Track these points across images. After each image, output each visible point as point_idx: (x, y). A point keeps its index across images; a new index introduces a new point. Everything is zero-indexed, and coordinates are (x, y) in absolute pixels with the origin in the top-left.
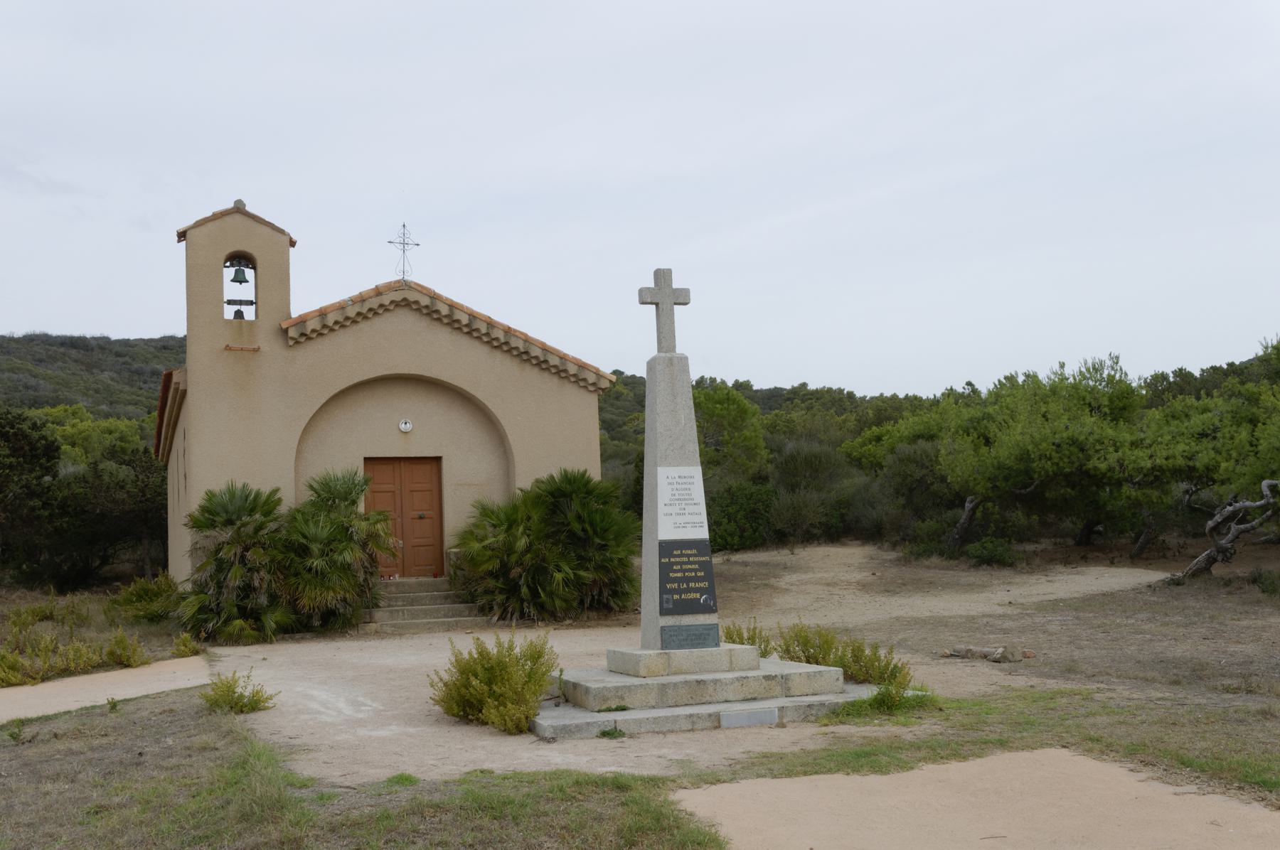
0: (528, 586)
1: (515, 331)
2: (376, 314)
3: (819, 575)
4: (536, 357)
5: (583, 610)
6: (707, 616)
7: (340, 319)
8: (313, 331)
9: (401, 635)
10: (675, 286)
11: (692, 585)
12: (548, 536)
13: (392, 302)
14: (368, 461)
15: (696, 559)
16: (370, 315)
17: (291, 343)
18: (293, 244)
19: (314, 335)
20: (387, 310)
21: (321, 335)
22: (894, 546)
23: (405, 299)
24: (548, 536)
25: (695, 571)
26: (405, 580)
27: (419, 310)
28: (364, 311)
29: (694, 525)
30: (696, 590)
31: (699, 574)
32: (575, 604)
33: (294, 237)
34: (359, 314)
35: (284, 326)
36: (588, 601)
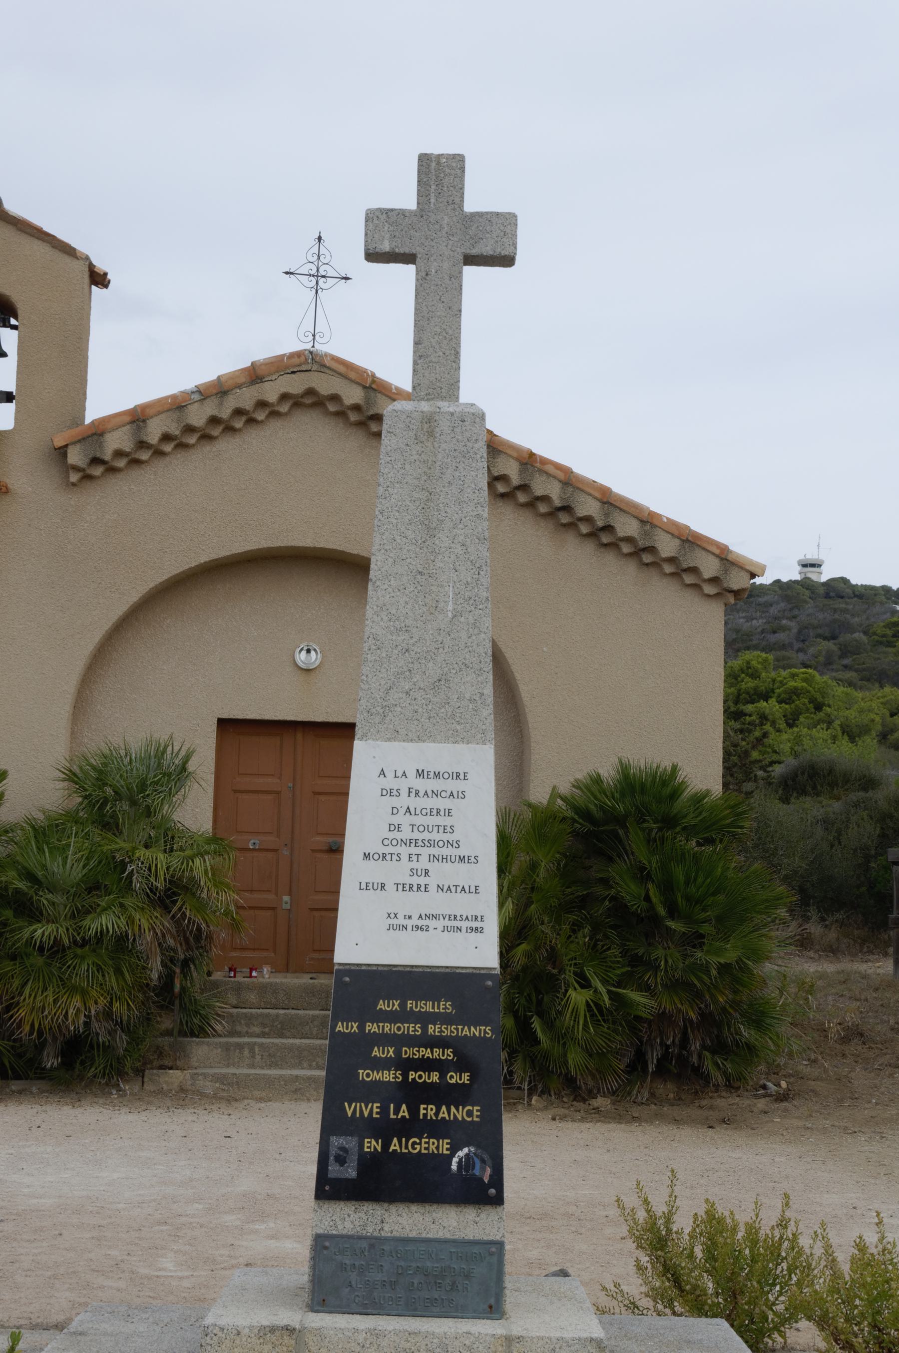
1: (545, 461)
2: (251, 421)
4: (588, 519)
7: (174, 430)
8: (119, 454)
9: (230, 1100)
10: (471, 205)
13: (284, 397)
14: (223, 723)
15: (448, 1031)
16: (238, 424)
17: (74, 477)
18: (99, 279)
19: (121, 463)
20: (274, 414)
21: (136, 462)
23: (310, 392)
26: (280, 979)
27: (341, 414)
28: (225, 414)
29: (455, 923)
31: (454, 1078)
33: (101, 265)
34: (214, 421)
35: (59, 442)
36: (653, 1058)
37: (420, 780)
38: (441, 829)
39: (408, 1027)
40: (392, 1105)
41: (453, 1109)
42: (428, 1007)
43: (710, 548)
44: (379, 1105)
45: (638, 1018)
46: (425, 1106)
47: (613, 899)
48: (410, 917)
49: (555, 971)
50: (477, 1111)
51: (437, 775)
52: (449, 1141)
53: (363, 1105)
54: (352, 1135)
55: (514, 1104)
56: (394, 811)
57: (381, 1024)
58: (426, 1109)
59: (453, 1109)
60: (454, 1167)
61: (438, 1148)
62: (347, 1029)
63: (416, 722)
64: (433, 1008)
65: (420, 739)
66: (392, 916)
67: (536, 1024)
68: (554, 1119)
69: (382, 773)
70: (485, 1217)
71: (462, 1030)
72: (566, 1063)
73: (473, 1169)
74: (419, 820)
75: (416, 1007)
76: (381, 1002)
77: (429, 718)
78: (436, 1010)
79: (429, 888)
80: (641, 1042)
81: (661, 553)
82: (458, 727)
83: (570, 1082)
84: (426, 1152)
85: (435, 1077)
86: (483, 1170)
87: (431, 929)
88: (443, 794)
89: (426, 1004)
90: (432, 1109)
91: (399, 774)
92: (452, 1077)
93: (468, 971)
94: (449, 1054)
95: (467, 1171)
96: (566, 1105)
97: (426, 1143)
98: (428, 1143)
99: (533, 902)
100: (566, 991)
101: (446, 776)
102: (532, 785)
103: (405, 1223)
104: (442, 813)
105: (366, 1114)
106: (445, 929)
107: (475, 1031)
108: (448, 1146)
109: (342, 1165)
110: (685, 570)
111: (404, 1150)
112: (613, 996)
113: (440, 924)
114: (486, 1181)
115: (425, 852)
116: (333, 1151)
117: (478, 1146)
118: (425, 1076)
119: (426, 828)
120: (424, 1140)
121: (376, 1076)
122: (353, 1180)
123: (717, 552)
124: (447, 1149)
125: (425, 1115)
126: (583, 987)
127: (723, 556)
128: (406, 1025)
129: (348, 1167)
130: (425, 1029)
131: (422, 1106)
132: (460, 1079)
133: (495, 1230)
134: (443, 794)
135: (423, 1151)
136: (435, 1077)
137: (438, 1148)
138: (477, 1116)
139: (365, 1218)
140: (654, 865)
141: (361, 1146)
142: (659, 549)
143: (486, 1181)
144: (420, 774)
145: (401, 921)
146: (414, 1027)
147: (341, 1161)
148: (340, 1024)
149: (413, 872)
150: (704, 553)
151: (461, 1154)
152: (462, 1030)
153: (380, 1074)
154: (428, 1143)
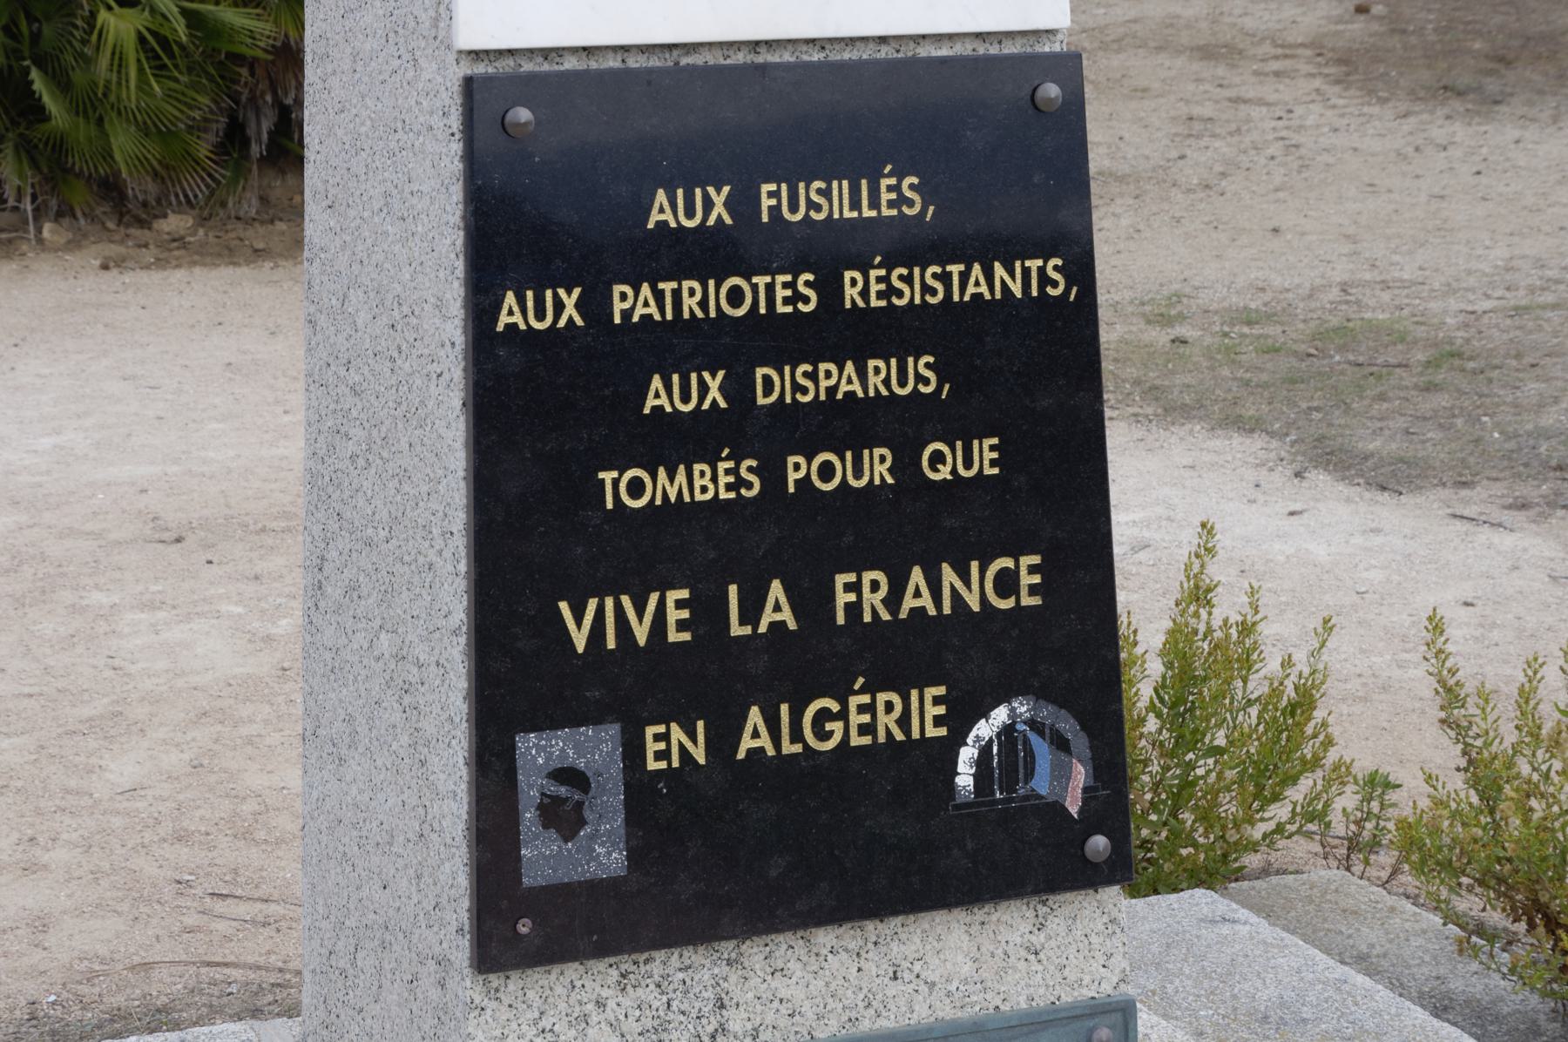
5: (240, 172)
6: (1012, 923)
11: (861, 593)
15: (918, 287)
25: (896, 422)
30: (898, 654)
31: (944, 464)
32: (203, 150)
39: (770, 288)
40: (733, 590)
41: (949, 575)
42: (832, 202)
44: (684, 594)
46: (851, 577)
50: (1032, 570)
52: (941, 690)
53: (626, 600)
54: (597, 720)
55: (10, 241)
57: (667, 287)
58: (855, 587)
59: (949, 575)
60: (965, 779)
61: (905, 722)
62: (540, 316)
64: (855, 204)
67: (38, 83)
68: (105, 267)
70: (1062, 930)
71: (965, 277)
72: (108, 155)
73: (1030, 774)
75: (794, 208)
76: (661, 196)
78: (868, 213)
80: (237, 103)
83: (111, 189)
84: (866, 740)
85: (879, 466)
86: (1061, 775)
89: (826, 193)
90: (875, 586)
92: (937, 458)
93: (959, 49)
94: (921, 375)
95: (1009, 787)
96: (117, 237)
97: (862, 709)
98: (869, 708)
100: (93, 15)
103: (798, 994)
105: (641, 634)
107: (1008, 280)
108: (941, 710)
109: (569, 834)
111: (789, 748)
114: (1074, 810)
116: (532, 787)
117: (1041, 693)
118: (843, 468)
120: (854, 701)
121: (667, 486)
122: (614, 883)
124: (938, 721)
125: (854, 609)
128: (761, 281)
129: (593, 837)
130: (829, 288)
131: (841, 579)
132: (968, 464)
133: (1096, 966)
135: (856, 741)
136: (879, 466)
137: (905, 722)
138: (1033, 590)
139: (659, 1002)
141: (633, 751)
143: (1074, 810)
146: (790, 285)
147: (563, 818)
148: (510, 298)
151: (984, 729)
152: (965, 277)
153: (681, 477)
154: (869, 708)
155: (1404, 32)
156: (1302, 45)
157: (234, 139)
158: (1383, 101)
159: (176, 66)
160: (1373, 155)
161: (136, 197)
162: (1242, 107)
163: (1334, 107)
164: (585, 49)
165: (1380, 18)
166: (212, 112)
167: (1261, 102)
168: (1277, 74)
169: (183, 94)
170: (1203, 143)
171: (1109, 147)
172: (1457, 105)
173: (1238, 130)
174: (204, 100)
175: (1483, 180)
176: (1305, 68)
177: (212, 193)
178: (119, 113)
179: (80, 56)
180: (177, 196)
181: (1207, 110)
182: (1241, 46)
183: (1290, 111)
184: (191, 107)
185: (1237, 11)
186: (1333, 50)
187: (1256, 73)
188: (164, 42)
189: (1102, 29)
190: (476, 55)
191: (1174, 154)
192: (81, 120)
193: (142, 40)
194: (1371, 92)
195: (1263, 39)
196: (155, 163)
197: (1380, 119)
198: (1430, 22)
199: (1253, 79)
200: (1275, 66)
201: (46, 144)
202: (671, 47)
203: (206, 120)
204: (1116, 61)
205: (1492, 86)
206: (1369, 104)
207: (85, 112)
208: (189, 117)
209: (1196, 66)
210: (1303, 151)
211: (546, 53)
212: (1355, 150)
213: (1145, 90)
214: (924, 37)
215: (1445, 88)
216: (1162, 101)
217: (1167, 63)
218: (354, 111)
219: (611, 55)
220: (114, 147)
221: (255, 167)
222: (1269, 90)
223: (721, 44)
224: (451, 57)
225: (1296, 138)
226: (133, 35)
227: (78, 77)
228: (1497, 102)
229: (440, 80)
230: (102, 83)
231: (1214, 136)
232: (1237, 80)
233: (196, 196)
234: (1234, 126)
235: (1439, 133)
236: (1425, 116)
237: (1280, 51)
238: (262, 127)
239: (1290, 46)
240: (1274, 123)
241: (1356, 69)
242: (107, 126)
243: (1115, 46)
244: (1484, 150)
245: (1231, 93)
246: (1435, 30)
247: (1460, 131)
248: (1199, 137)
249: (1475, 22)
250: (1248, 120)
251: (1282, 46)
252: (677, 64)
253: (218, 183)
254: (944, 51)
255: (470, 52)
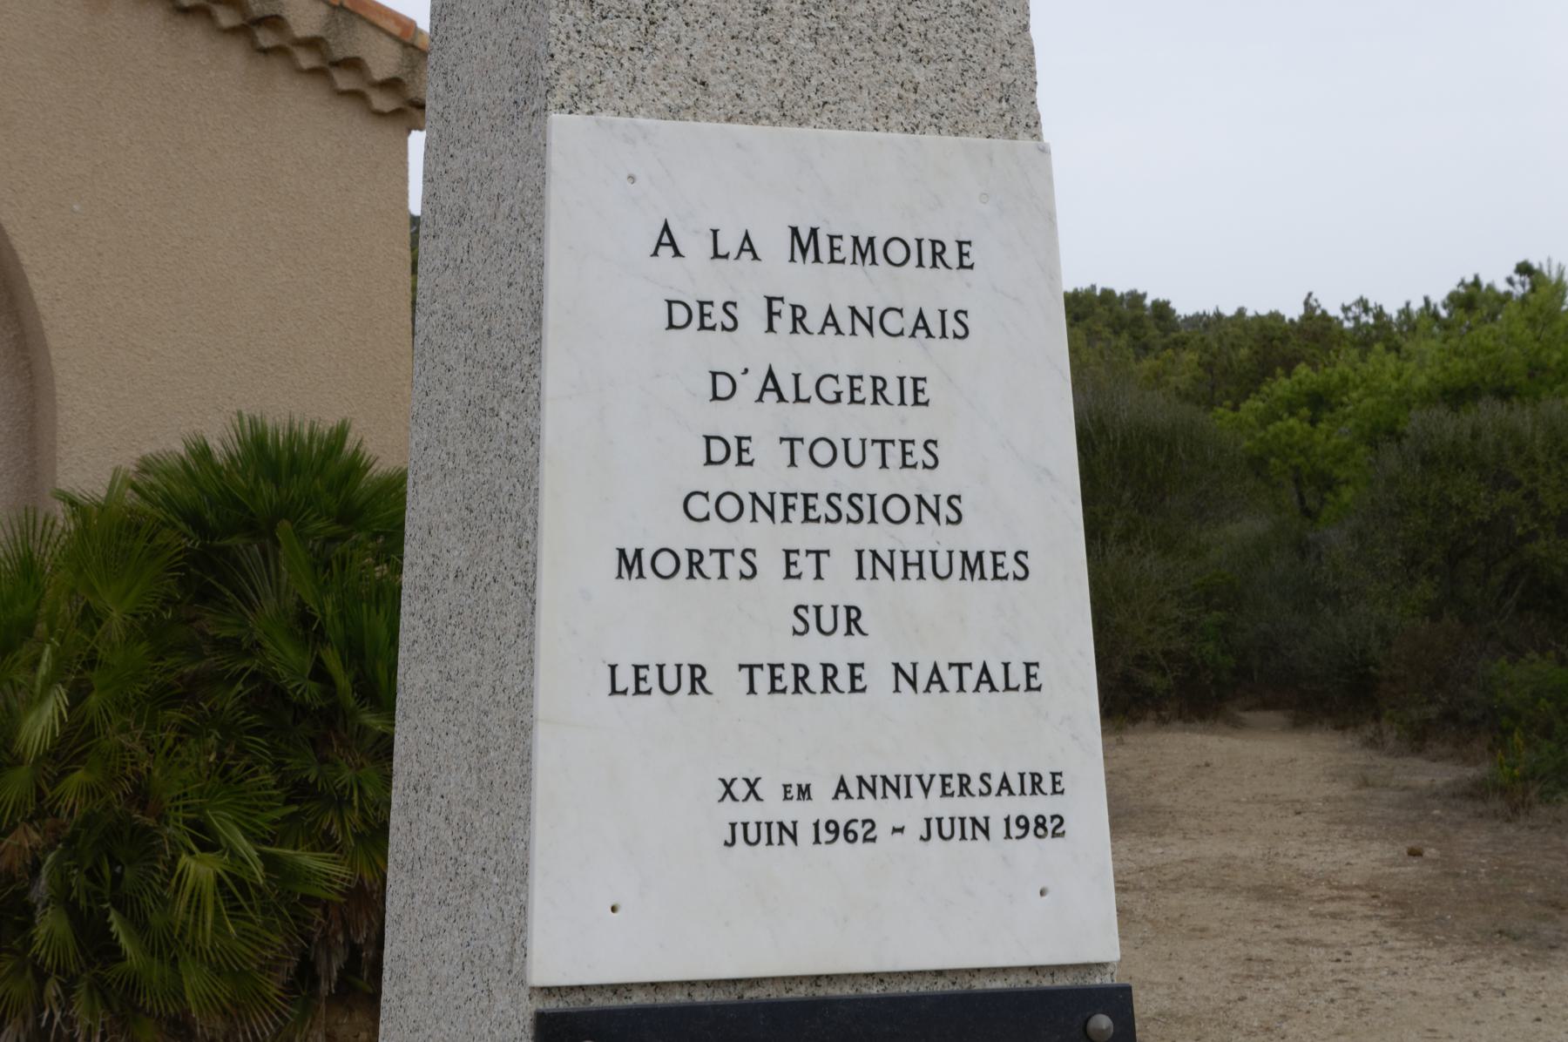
0: (71, 909)
3: (1213, 848)
12: (165, 697)
22: (1418, 739)
24: (165, 697)
29: (992, 808)
32: (273, 989)
37: (805, 269)
38: (894, 452)
43: (384, 23)
45: (309, 900)
47: (255, 676)
48: (804, 792)
49: (150, 822)
51: (865, 250)
56: (721, 386)
63: (767, 50)
65: (785, 114)
66: (740, 789)
69: (667, 239)
72: (179, 994)
74: (812, 420)
77: (815, 35)
79: (866, 677)
81: (294, 28)
82: (920, 74)
87: (882, 831)
88: (892, 322)
91: (729, 243)
99: (90, 690)
100: (175, 859)
101: (897, 251)
102: (60, 468)
104: (892, 392)
106: (933, 829)
110: (337, 64)
112: (270, 862)
113: (913, 810)
115: (843, 540)
119: (841, 451)
123: (397, 31)
126: (204, 847)
127: (408, 40)
134: (892, 322)
140: (329, 609)
142: (290, 20)
144: (804, 243)
145: (774, 808)
149: (806, 618)
150: (371, 32)
155: (1458, 875)
156: (1358, 887)
157: (306, 975)
158: (1440, 945)
159: (252, 908)
160: (1432, 999)
161: (203, 1035)
162: (1300, 948)
163: (1392, 949)
164: (652, 984)
165: (1435, 861)
166: (284, 951)
167: (1319, 944)
168: (1334, 915)
169: (257, 934)
170: (1262, 985)
171: (1170, 987)
172: (1513, 949)
173: (1297, 972)
174: (277, 940)
175: (1544, 1027)
176: (1361, 910)
177: (280, 1030)
178: (194, 953)
179: (160, 898)
180: (245, 1033)
181: (1265, 951)
182: (1297, 887)
183: (1349, 954)
184: (263, 946)
185: (1293, 852)
186: (1388, 892)
187: (1312, 914)
188: (241, 885)
189: (1159, 868)
190: (549, 991)
191: (1234, 995)
192: (156, 960)
193: (220, 882)
194: (1427, 936)
195: (1319, 880)
196: (224, 1001)
197: (1437, 963)
198: (1483, 866)
199: (1311, 921)
200: (1332, 907)
201: (120, 983)
202: (735, 982)
203: (277, 959)
204: (1174, 900)
205: (1547, 930)
206: (1426, 948)
207: (160, 952)
208: (261, 956)
209: (1254, 906)
210: (1362, 994)
211: (615, 989)
212: (1414, 993)
213: (1203, 930)
214: (979, 970)
215: (1501, 932)
216: (1221, 941)
217: (1225, 903)
218: (428, 1032)
219: (677, 989)
220: (187, 988)
221: (323, 1005)
222: (1324, 932)
223: (783, 979)
224: (524, 993)
225: (1355, 981)
226: (212, 878)
227: (156, 919)
228: (1552, 947)
229: (513, 1012)
230: (178, 924)
231: (1273, 977)
232: (1295, 921)
233: (263, 1034)
234: (1292, 968)
235: (1497, 978)
236: (1482, 961)
237: (1335, 892)
238: (332, 966)
239: (1346, 888)
240: (1333, 965)
241: (1412, 913)
242: (180, 966)
243: (1173, 886)
244: (1543, 997)
245: (1290, 934)
246: (1488, 874)
247: (1518, 977)
248: (1258, 978)
249: (1527, 867)
250: (1307, 962)
251: (1337, 888)
252: (741, 997)
253: (286, 1020)
254: (998, 984)
255: (542, 988)
